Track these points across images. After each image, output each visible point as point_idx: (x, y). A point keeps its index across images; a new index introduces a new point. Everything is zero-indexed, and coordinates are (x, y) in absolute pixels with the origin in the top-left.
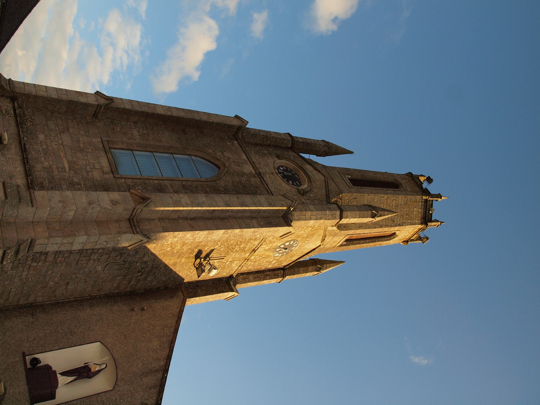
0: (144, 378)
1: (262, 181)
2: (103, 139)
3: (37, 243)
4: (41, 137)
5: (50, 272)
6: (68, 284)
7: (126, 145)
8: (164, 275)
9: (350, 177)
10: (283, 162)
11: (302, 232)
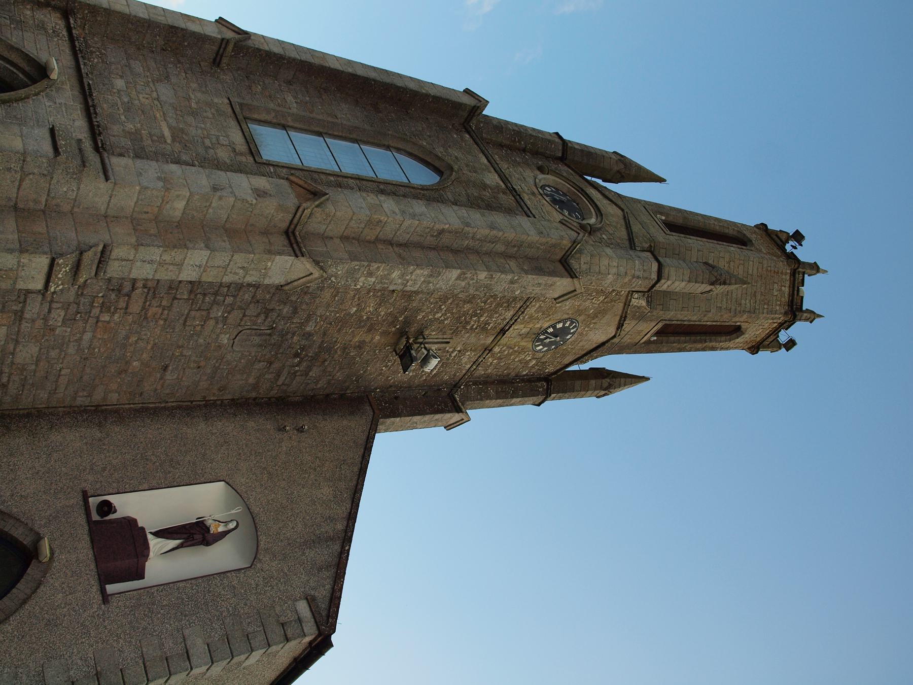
0: (307, 551)
1: (519, 200)
2: (235, 100)
3: (114, 255)
4: (120, 83)
5: (133, 339)
6: (165, 368)
7: (273, 114)
8: (340, 369)
9: (663, 218)
10: (550, 179)
11: (588, 303)
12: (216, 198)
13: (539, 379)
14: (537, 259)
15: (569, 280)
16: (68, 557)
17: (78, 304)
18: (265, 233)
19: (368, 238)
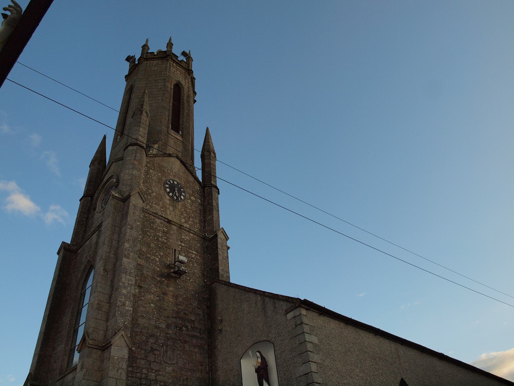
0: (269, 315)
7: (65, 357)
13: (204, 192)
14: (123, 215)
15: (131, 198)
18: (102, 361)
19: (108, 307)
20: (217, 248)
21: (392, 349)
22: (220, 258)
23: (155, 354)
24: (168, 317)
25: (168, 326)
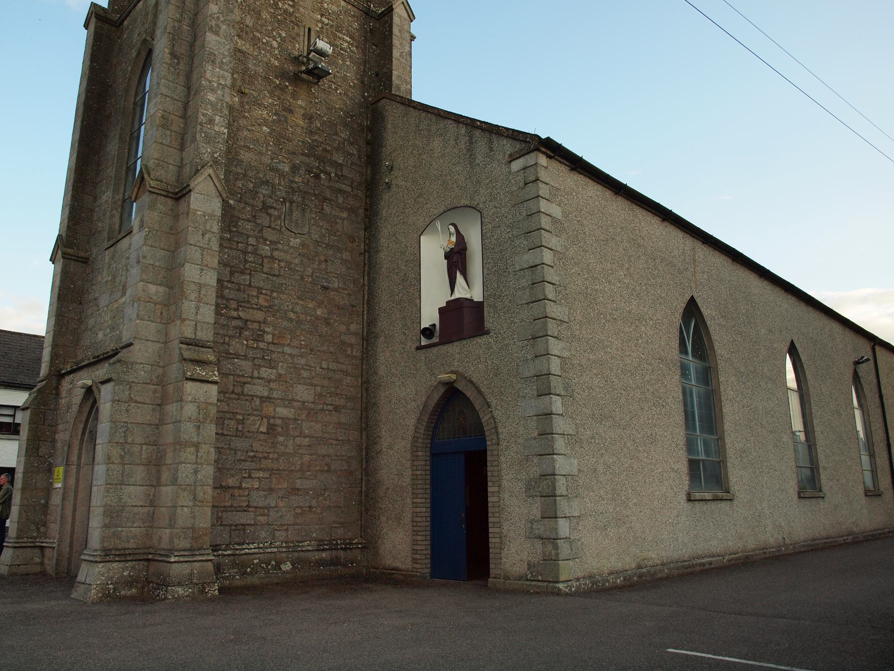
0: (477, 161)
5: (292, 315)
6: (325, 288)
7: (114, 212)
8: (336, 134)
12: (144, 261)
16: (466, 359)
17: (254, 358)
18: (176, 217)
19: (182, 125)
20: (391, 31)
21: (686, 248)
22: (396, 53)
23: (270, 215)
24: (295, 154)
25: (294, 169)
